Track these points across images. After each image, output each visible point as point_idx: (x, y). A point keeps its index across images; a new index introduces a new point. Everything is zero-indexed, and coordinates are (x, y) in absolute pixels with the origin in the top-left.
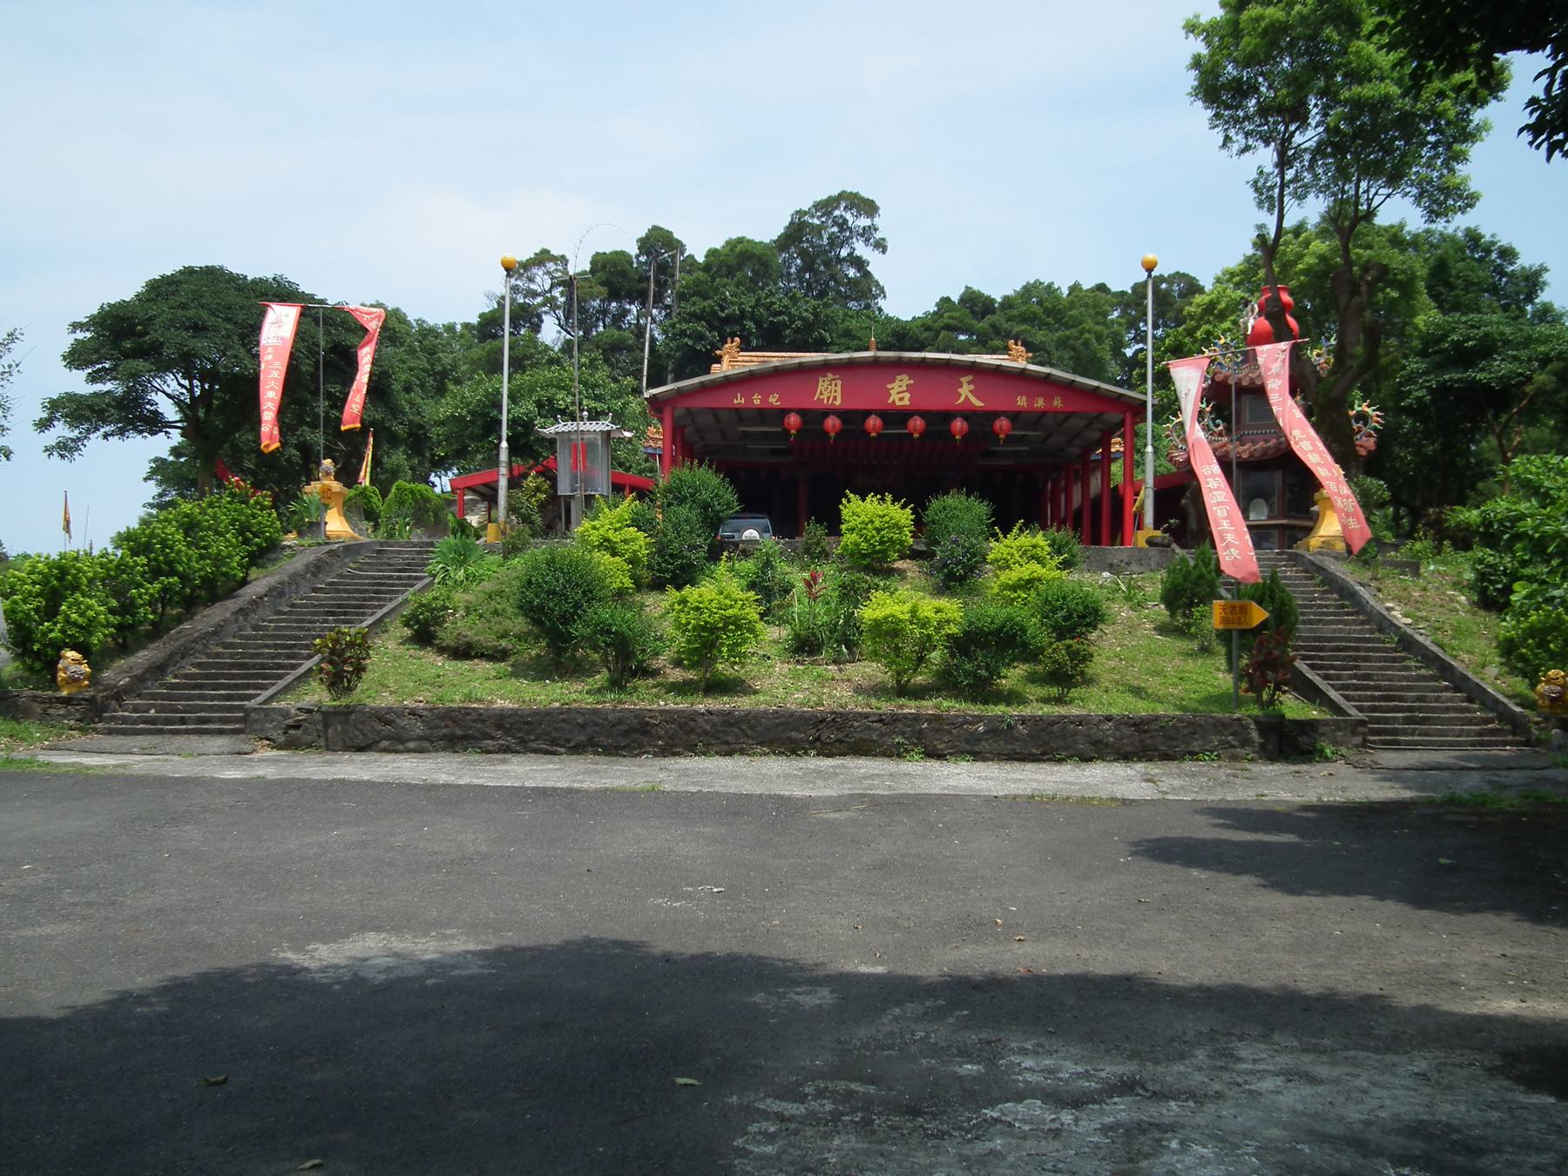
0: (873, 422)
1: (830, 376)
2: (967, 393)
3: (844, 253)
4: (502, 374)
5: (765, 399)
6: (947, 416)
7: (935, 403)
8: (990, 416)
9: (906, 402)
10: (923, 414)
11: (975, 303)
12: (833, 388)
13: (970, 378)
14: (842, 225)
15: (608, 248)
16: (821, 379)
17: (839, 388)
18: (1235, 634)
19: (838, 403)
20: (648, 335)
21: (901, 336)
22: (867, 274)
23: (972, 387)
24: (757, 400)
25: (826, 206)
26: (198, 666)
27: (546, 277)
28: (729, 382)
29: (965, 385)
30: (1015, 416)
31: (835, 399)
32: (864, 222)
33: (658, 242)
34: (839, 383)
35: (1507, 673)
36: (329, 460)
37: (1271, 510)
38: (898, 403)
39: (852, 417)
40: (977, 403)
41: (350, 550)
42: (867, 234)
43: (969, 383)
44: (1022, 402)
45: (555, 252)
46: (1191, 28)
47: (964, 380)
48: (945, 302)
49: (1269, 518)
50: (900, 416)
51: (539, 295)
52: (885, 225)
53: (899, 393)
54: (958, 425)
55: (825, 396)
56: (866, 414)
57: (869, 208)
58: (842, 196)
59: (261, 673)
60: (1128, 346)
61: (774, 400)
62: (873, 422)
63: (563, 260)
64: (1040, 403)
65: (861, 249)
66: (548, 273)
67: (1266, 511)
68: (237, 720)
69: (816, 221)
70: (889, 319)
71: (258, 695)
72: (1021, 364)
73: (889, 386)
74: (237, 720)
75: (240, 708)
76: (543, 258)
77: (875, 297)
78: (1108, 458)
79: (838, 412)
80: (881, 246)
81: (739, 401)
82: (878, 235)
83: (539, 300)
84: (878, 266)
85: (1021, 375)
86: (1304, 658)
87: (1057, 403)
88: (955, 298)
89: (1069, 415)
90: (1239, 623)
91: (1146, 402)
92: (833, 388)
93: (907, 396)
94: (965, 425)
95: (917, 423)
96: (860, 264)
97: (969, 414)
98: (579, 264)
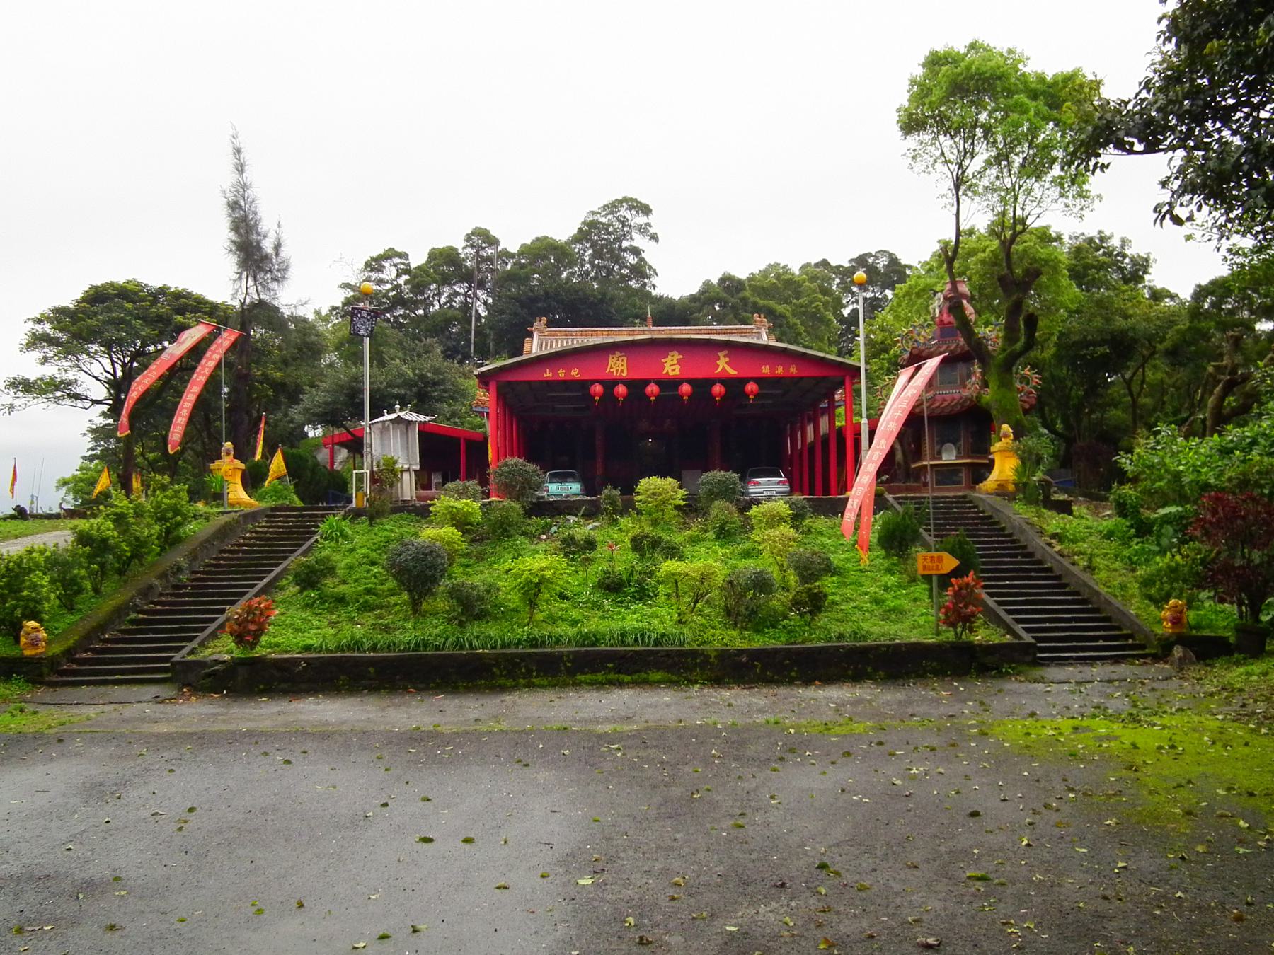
0: (652, 389)
1: (618, 354)
2: (723, 365)
3: (625, 244)
4: (362, 364)
5: (566, 374)
6: (711, 382)
7: (700, 373)
8: (743, 381)
9: (677, 373)
10: (690, 381)
11: (729, 284)
12: (620, 363)
13: (726, 352)
14: (623, 222)
15: (441, 245)
16: (611, 357)
17: (625, 363)
18: (935, 579)
19: (624, 374)
20: (474, 313)
21: (672, 313)
22: (642, 260)
23: (727, 359)
24: (562, 374)
25: (613, 207)
26: (132, 622)
27: (393, 268)
28: (540, 361)
29: (722, 358)
30: (759, 380)
31: (622, 371)
32: (641, 220)
33: (482, 237)
34: (625, 359)
35: (1052, 254)
36: (229, 443)
37: (959, 452)
38: (671, 373)
39: (637, 386)
40: (732, 372)
41: (252, 516)
42: (644, 229)
43: (725, 356)
44: (766, 370)
45: (398, 249)
46: (939, 241)
47: (721, 354)
48: (707, 285)
49: (958, 458)
50: (675, 383)
51: (387, 282)
52: (656, 222)
53: (672, 366)
54: (718, 389)
55: (614, 370)
56: (646, 382)
57: (646, 210)
58: (625, 200)
59: (185, 629)
60: (844, 306)
61: (575, 374)
62: (652, 389)
63: (403, 256)
64: (780, 370)
65: (638, 241)
66: (395, 265)
67: (955, 453)
68: (165, 670)
69: (604, 220)
70: (660, 299)
71: (184, 647)
72: (765, 339)
73: (664, 361)
74: (165, 670)
75: (167, 659)
76: (389, 255)
77: (649, 277)
78: (832, 407)
79: (626, 382)
80: (654, 238)
81: (548, 375)
82: (652, 231)
83: (389, 286)
84: (652, 253)
85: (766, 349)
86: (985, 587)
87: (793, 370)
88: (715, 281)
89: (801, 378)
90: (938, 569)
91: (859, 368)
92: (620, 363)
93: (678, 368)
94: (723, 389)
95: (686, 388)
96: (636, 251)
97: (725, 381)
98: (418, 259)
